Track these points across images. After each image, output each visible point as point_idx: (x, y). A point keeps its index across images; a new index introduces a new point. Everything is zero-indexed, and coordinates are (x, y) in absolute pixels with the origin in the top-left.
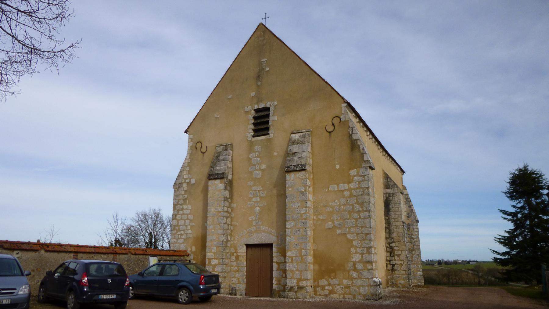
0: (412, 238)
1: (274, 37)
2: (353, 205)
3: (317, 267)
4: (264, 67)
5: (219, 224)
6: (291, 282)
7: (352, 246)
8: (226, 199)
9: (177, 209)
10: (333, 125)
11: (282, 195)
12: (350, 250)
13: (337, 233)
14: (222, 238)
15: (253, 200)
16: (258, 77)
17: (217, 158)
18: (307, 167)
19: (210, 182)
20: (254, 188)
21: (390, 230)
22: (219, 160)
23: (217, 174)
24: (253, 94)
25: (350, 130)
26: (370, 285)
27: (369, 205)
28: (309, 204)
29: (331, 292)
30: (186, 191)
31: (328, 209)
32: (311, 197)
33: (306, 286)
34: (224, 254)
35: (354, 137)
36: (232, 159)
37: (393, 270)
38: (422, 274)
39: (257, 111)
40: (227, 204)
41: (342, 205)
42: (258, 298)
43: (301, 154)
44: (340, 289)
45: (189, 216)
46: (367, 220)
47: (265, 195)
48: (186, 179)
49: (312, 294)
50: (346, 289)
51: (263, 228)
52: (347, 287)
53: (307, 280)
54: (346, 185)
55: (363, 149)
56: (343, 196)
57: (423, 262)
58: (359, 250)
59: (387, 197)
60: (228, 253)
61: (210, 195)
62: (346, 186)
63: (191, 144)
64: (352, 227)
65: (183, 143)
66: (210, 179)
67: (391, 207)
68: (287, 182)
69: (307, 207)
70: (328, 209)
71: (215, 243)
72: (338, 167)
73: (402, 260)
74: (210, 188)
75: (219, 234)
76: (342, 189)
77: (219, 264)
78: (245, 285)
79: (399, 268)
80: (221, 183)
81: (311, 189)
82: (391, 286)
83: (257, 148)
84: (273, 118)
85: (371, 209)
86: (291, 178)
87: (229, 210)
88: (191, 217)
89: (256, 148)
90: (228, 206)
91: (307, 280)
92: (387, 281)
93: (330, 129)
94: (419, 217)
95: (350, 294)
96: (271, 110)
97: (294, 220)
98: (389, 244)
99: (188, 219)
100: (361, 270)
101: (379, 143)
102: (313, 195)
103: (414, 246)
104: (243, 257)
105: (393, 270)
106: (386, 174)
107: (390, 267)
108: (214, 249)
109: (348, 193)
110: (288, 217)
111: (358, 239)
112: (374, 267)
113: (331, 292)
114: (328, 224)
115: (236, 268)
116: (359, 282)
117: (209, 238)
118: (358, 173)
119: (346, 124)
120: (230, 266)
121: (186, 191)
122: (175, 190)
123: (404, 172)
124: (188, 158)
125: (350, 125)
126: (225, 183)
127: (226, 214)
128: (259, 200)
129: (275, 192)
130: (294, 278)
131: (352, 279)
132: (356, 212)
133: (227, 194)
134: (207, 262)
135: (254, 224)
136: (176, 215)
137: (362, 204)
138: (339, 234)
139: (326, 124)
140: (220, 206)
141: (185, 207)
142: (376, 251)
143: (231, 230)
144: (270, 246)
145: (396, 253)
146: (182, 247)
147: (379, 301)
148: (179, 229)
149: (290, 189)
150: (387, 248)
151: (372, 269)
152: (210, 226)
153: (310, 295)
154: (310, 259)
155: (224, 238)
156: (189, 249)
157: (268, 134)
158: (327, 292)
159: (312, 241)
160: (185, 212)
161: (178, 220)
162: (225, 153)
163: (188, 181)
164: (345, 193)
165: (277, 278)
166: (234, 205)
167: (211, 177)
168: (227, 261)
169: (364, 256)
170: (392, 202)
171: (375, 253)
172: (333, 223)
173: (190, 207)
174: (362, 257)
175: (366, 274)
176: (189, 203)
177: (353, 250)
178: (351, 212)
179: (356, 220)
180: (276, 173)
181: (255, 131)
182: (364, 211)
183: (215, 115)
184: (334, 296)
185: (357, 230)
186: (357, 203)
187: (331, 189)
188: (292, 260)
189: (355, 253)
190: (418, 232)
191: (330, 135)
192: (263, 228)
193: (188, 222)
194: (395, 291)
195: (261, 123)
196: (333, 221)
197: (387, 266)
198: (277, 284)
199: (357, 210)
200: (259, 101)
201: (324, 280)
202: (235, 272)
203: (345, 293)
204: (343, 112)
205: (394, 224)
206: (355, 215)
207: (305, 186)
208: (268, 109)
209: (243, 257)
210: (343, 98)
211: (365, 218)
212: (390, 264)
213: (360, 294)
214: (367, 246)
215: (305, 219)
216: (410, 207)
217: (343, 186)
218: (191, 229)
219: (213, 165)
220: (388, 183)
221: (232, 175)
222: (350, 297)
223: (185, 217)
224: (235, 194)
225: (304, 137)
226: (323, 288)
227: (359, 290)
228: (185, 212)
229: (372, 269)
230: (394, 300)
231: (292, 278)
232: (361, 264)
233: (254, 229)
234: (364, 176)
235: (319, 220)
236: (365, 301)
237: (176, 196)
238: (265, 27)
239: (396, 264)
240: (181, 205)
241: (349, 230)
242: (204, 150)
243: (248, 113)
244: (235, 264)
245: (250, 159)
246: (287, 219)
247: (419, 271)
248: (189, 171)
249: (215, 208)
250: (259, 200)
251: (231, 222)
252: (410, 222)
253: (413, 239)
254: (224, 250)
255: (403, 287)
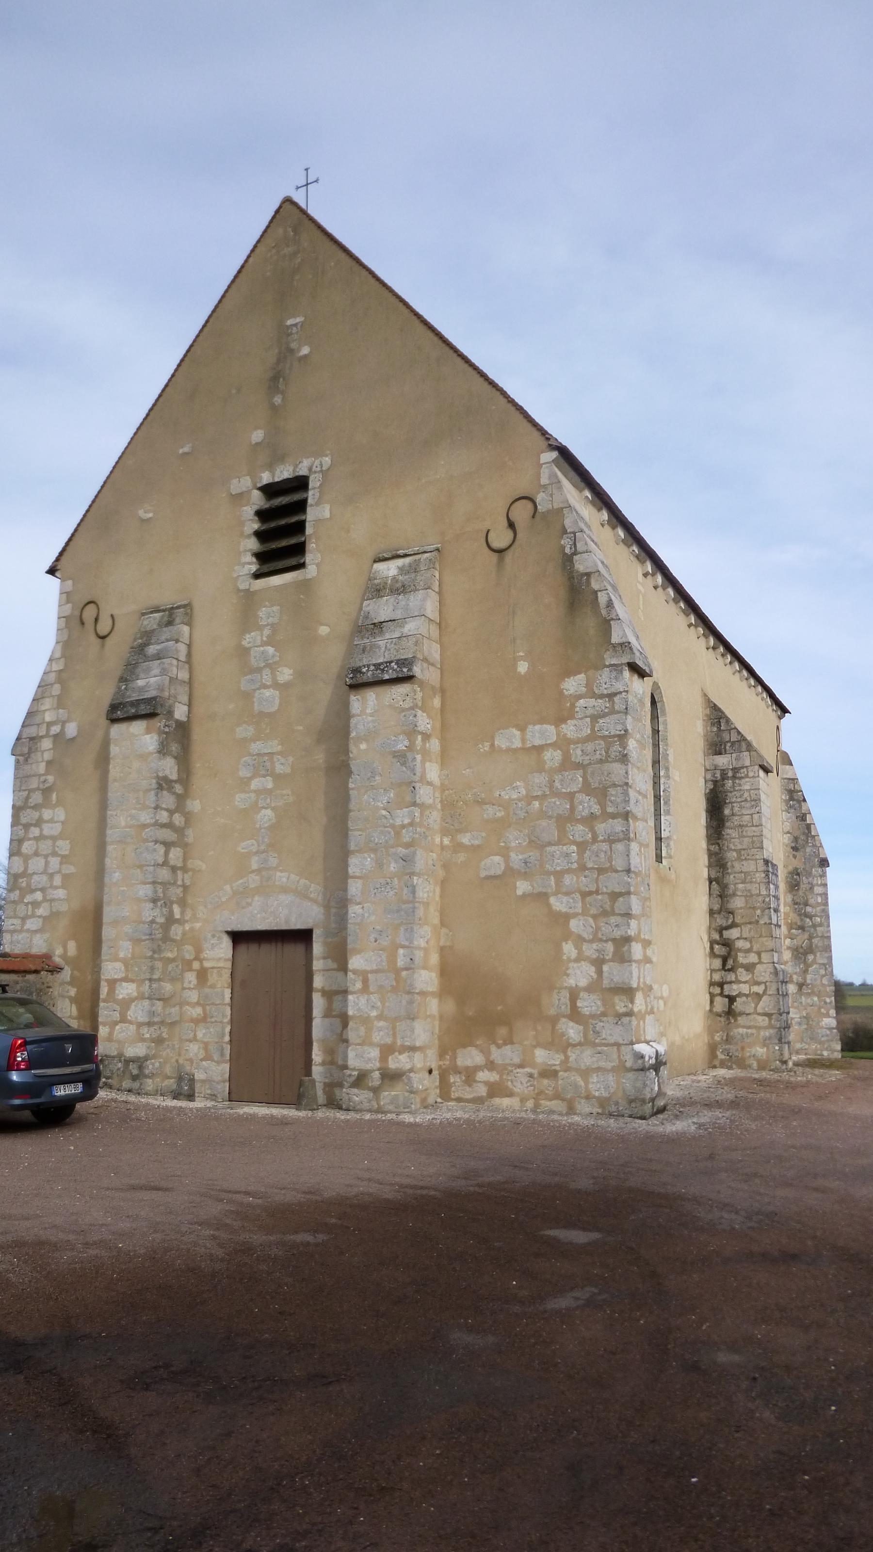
0: (807, 915)
1: (328, 243)
2: (571, 796)
3: (450, 1006)
4: (294, 345)
5: (140, 867)
6: (361, 1057)
7: (567, 935)
8: (163, 784)
9: (24, 820)
10: (511, 525)
11: (340, 769)
12: (559, 950)
13: (519, 892)
14: (148, 912)
15: (255, 784)
16: (276, 380)
17: (139, 653)
18: (417, 670)
19: (117, 730)
20: (256, 747)
21: (724, 887)
22: (147, 659)
23: (136, 703)
24: (258, 436)
25: (566, 542)
26: (621, 1068)
27: (626, 794)
28: (425, 794)
29: (496, 1090)
30: (49, 763)
31: (491, 812)
32: (433, 772)
33: (411, 1070)
34: (159, 965)
35: (580, 566)
36: (189, 655)
37: (730, 1013)
38: (833, 1023)
39: (269, 491)
40: (168, 800)
41: (536, 798)
42: (276, 1111)
43: (402, 626)
44: (525, 1080)
45: (60, 843)
46: (620, 847)
47: (288, 770)
48: (50, 724)
49: (433, 1096)
50: (546, 1082)
51: (281, 877)
52: (549, 1073)
53: (413, 1049)
54: (551, 729)
55: (610, 604)
56: (540, 768)
57: (841, 990)
58: (590, 950)
59: (715, 782)
60: (173, 960)
61: (114, 771)
62: (550, 732)
63: (68, 609)
64: (569, 871)
65: (38, 610)
66: (114, 721)
67: (727, 812)
68: (353, 721)
69: (414, 804)
70: (491, 812)
71: (128, 928)
72: (523, 667)
73: (758, 983)
74: (114, 750)
75: (139, 900)
76: (538, 742)
77: (141, 997)
78: (227, 1066)
79: (750, 1009)
80: (148, 731)
81: (434, 745)
82: (723, 1064)
83: (267, 614)
84: (318, 513)
85: (632, 807)
86: (367, 706)
87: (178, 820)
88: (64, 846)
89: (262, 613)
90: (172, 807)
91: (413, 1049)
92: (712, 1049)
93: (501, 538)
94: (829, 850)
95: (557, 1096)
96: (311, 486)
97: (374, 851)
98: (721, 930)
99: (54, 854)
100: (593, 1016)
101: (692, 607)
102: (443, 765)
103: (810, 938)
104: (220, 975)
105: (730, 1013)
106: (715, 708)
107: (720, 1004)
108: (125, 949)
109: (558, 755)
110: (356, 838)
111: (585, 912)
112: (639, 1003)
113: (496, 1090)
114: (488, 861)
115: (199, 1010)
116: (587, 1058)
117: (109, 913)
118: (589, 685)
119: (553, 521)
120: (181, 1004)
121: (49, 763)
122: (17, 762)
123: (784, 710)
124: (58, 655)
125: (568, 523)
126: (160, 732)
127: (168, 835)
128: (270, 785)
129: (319, 757)
130: (371, 1044)
131: (565, 1046)
132: (584, 821)
133: (169, 767)
134: (104, 990)
135: (255, 866)
136: (20, 841)
137: (601, 794)
138: (524, 896)
139: (487, 525)
140: (144, 807)
141: (47, 814)
142: (649, 952)
143: (185, 888)
144: (304, 936)
145: (741, 959)
146: (38, 945)
147: (654, 1121)
148: (29, 885)
149: (363, 746)
150: (712, 943)
151: (630, 1014)
152: (114, 876)
153: (424, 1100)
154: (427, 979)
155: (157, 912)
156: (59, 951)
157: (302, 566)
158: (482, 1091)
159: (436, 921)
160: (47, 830)
161: (26, 858)
162: (167, 633)
163: (55, 729)
164: (548, 755)
165: (323, 1041)
166: (194, 805)
167: (121, 712)
168: (168, 987)
169: (605, 968)
170: (732, 797)
171: (648, 960)
172: (506, 858)
173: (60, 814)
174: (600, 972)
175: (610, 1032)
176: (59, 803)
177: (569, 949)
178: (563, 821)
179: (582, 846)
180: (324, 693)
181: (262, 557)
182: (607, 816)
183: (141, 513)
184: (506, 1102)
185: (585, 882)
186: (587, 789)
187: (501, 742)
188: (365, 982)
189: (577, 960)
190: (825, 895)
191: (501, 561)
192: (281, 877)
193: (54, 862)
194: (731, 1082)
195: (281, 534)
196: (504, 852)
197: (712, 1002)
198: (323, 1063)
199: (585, 813)
200: (277, 458)
201: (474, 1051)
202: (196, 1021)
203: (541, 1093)
204: (544, 480)
205: (737, 867)
206: (579, 831)
207: (412, 732)
208: (300, 483)
209: (220, 975)
210: (543, 433)
211: (611, 840)
212: (721, 994)
213: (588, 1097)
214: (618, 934)
215: (408, 845)
216: (803, 817)
217: (542, 733)
218: (63, 887)
219: (127, 675)
220: (721, 734)
221: (190, 705)
222: (557, 1105)
223: (45, 847)
224: (198, 766)
225: (414, 569)
226: (469, 1076)
227: (587, 1083)
228: (47, 830)
229: (630, 1014)
230: (706, 1117)
231: (366, 1042)
232: (593, 997)
233: (254, 880)
234: (611, 696)
235: (458, 847)
236: (601, 1122)
237: (21, 779)
238: (304, 212)
239: (740, 995)
240: (36, 807)
241: (559, 882)
242: (104, 627)
243: (239, 498)
244: (194, 996)
245: (243, 652)
246: (352, 847)
247: (828, 1015)
248: (60, 697)
249: (132, 813)
250: (270, 785)
251: (185, 860)
252: (801, 866)
253: (811, 917)
254: (157, 950)
255: (762, 1066)
